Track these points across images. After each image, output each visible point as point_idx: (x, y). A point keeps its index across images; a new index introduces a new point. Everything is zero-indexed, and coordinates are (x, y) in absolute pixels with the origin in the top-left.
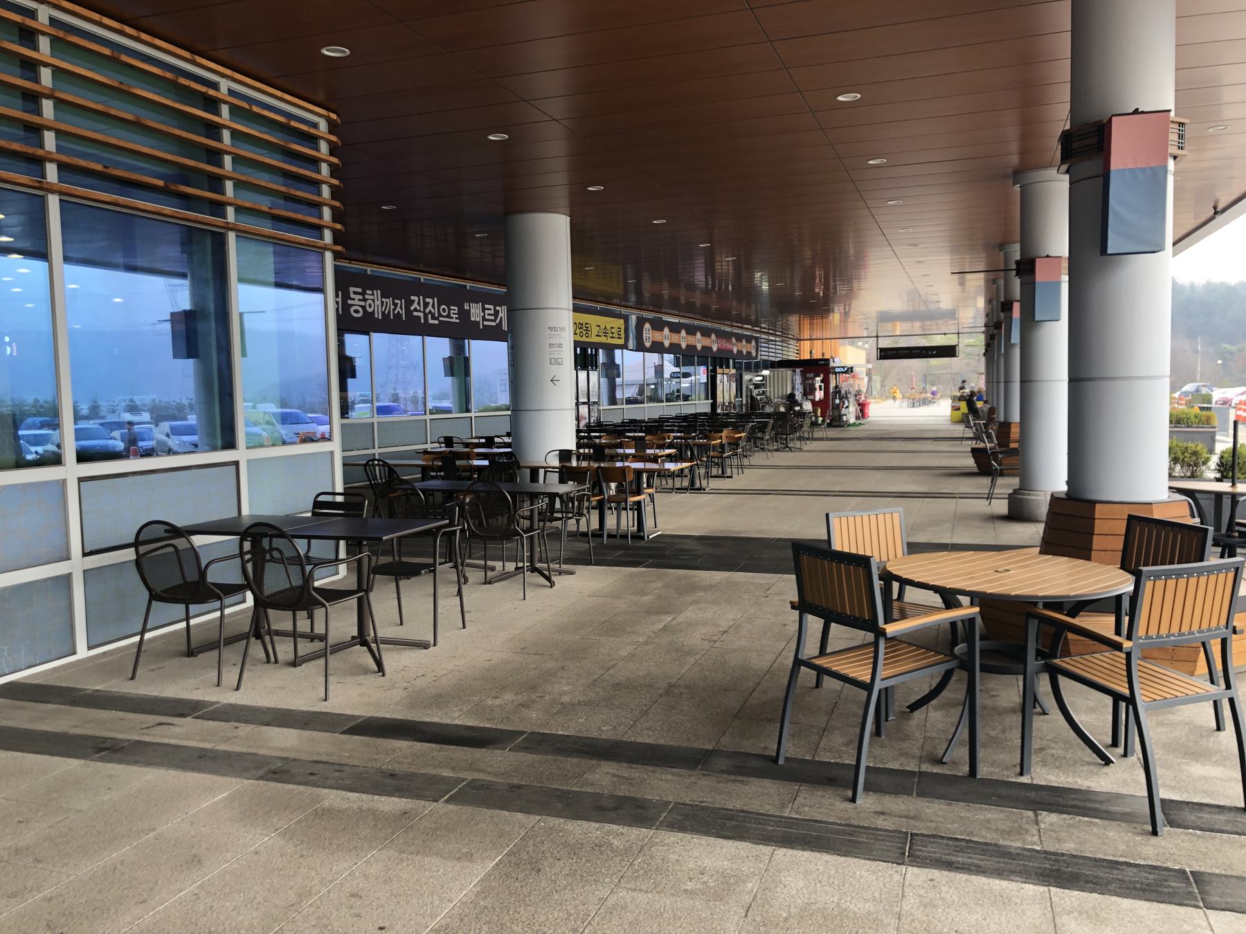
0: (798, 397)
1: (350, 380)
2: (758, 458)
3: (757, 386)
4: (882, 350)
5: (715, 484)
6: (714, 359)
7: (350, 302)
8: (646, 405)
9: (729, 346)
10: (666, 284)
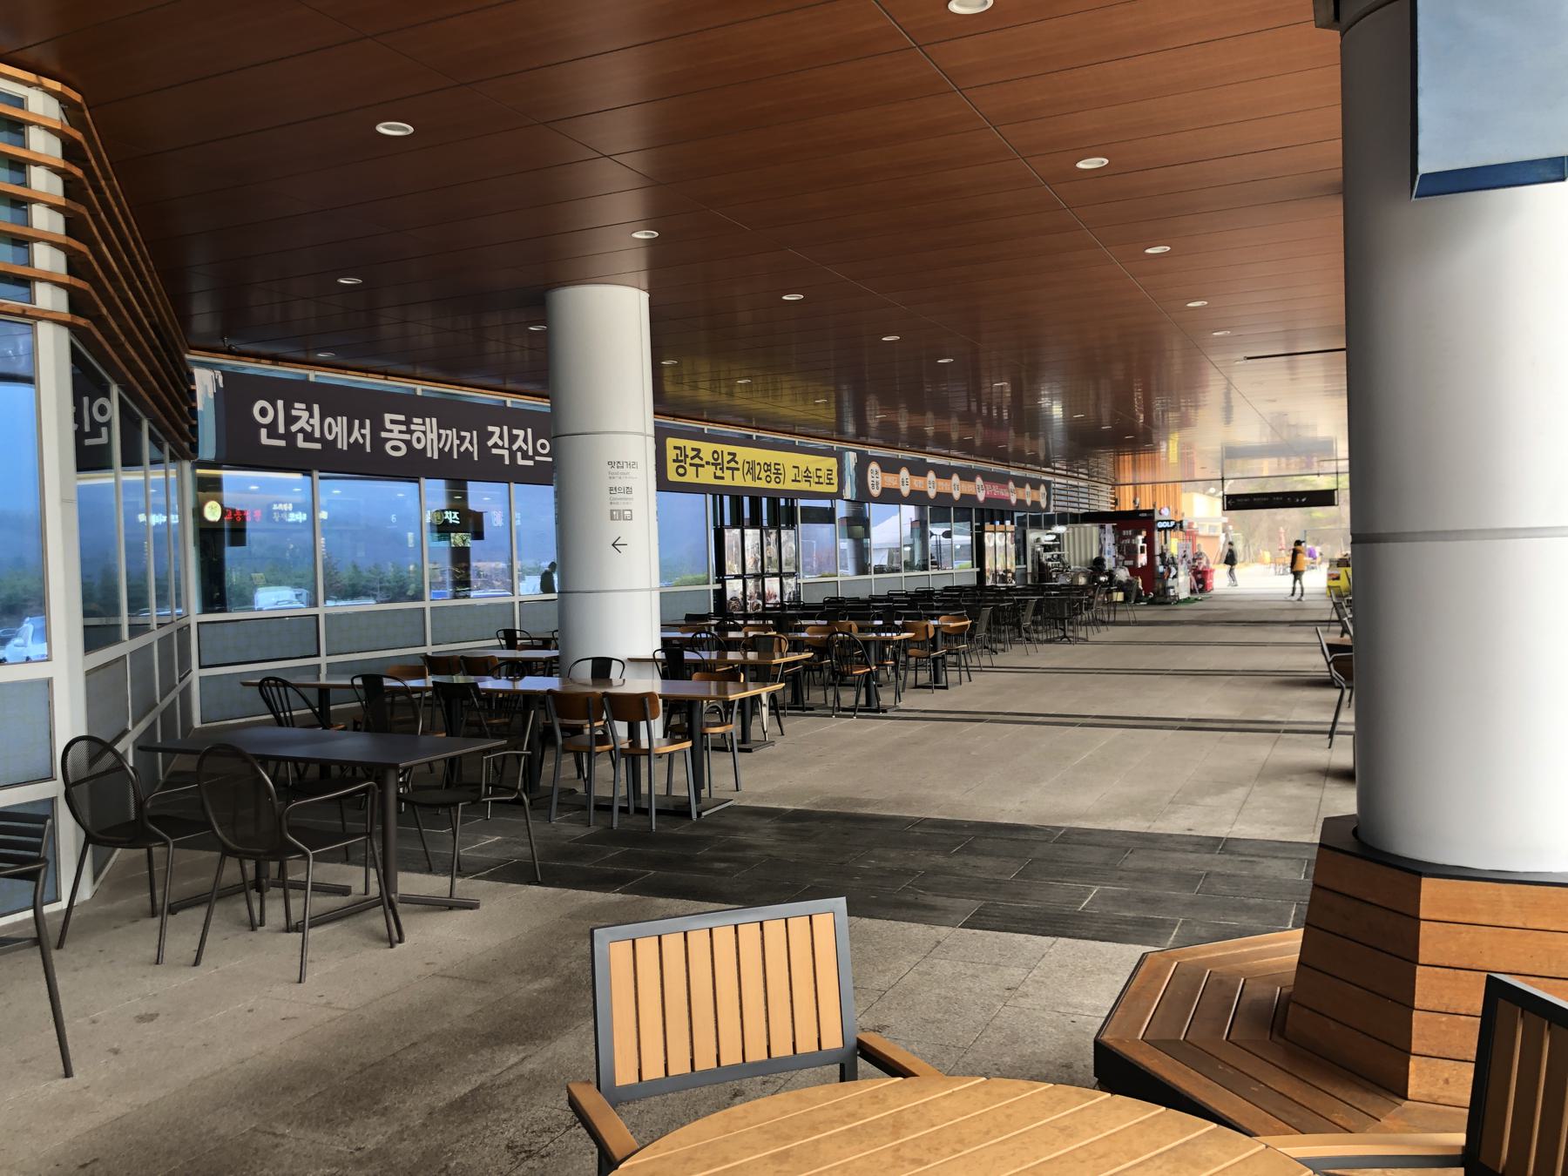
0: (1109, 564)
1: (229, 552)
2: (1015, 655)
3: (1047, 548)
4: (1229, 497)
5: (914, 700)
6: (981, 511)
7: (384, 435)
8: (903, 574)
9: (1003, 493)
10: (930, 415)
